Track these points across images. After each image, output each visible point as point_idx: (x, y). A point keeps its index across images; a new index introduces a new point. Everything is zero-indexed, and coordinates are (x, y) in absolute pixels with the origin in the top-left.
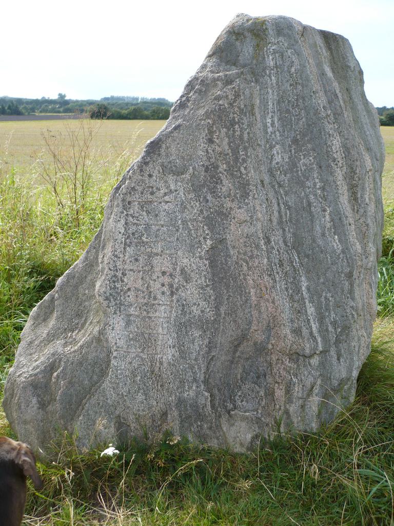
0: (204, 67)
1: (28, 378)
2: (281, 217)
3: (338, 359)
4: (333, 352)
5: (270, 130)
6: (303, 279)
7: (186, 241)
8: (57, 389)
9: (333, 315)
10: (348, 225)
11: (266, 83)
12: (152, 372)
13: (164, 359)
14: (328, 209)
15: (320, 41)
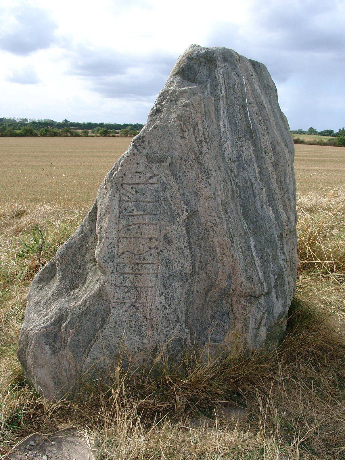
0: (171, 83)
1: (40, 330)
2: (233, 194)
3: (277, 298)
4: (273, 294)
5: (222, 129)
6: (251, 239)
7: (167, 213)
8: (66, 337)
9: (272, 266)
10: (277, 199)
11: (219, 96)
12: (144, 317)
13: (153, 306)
14: (264, 188)
15: (250, 68)
